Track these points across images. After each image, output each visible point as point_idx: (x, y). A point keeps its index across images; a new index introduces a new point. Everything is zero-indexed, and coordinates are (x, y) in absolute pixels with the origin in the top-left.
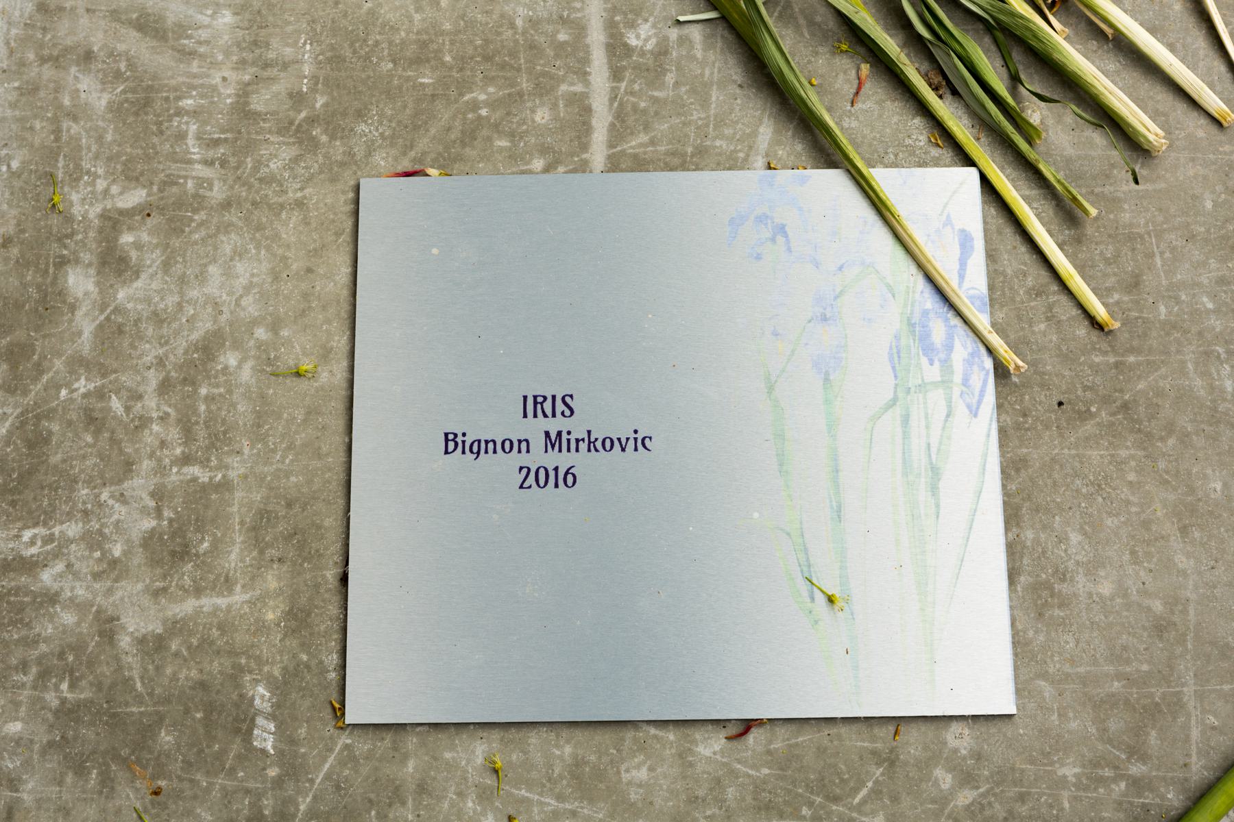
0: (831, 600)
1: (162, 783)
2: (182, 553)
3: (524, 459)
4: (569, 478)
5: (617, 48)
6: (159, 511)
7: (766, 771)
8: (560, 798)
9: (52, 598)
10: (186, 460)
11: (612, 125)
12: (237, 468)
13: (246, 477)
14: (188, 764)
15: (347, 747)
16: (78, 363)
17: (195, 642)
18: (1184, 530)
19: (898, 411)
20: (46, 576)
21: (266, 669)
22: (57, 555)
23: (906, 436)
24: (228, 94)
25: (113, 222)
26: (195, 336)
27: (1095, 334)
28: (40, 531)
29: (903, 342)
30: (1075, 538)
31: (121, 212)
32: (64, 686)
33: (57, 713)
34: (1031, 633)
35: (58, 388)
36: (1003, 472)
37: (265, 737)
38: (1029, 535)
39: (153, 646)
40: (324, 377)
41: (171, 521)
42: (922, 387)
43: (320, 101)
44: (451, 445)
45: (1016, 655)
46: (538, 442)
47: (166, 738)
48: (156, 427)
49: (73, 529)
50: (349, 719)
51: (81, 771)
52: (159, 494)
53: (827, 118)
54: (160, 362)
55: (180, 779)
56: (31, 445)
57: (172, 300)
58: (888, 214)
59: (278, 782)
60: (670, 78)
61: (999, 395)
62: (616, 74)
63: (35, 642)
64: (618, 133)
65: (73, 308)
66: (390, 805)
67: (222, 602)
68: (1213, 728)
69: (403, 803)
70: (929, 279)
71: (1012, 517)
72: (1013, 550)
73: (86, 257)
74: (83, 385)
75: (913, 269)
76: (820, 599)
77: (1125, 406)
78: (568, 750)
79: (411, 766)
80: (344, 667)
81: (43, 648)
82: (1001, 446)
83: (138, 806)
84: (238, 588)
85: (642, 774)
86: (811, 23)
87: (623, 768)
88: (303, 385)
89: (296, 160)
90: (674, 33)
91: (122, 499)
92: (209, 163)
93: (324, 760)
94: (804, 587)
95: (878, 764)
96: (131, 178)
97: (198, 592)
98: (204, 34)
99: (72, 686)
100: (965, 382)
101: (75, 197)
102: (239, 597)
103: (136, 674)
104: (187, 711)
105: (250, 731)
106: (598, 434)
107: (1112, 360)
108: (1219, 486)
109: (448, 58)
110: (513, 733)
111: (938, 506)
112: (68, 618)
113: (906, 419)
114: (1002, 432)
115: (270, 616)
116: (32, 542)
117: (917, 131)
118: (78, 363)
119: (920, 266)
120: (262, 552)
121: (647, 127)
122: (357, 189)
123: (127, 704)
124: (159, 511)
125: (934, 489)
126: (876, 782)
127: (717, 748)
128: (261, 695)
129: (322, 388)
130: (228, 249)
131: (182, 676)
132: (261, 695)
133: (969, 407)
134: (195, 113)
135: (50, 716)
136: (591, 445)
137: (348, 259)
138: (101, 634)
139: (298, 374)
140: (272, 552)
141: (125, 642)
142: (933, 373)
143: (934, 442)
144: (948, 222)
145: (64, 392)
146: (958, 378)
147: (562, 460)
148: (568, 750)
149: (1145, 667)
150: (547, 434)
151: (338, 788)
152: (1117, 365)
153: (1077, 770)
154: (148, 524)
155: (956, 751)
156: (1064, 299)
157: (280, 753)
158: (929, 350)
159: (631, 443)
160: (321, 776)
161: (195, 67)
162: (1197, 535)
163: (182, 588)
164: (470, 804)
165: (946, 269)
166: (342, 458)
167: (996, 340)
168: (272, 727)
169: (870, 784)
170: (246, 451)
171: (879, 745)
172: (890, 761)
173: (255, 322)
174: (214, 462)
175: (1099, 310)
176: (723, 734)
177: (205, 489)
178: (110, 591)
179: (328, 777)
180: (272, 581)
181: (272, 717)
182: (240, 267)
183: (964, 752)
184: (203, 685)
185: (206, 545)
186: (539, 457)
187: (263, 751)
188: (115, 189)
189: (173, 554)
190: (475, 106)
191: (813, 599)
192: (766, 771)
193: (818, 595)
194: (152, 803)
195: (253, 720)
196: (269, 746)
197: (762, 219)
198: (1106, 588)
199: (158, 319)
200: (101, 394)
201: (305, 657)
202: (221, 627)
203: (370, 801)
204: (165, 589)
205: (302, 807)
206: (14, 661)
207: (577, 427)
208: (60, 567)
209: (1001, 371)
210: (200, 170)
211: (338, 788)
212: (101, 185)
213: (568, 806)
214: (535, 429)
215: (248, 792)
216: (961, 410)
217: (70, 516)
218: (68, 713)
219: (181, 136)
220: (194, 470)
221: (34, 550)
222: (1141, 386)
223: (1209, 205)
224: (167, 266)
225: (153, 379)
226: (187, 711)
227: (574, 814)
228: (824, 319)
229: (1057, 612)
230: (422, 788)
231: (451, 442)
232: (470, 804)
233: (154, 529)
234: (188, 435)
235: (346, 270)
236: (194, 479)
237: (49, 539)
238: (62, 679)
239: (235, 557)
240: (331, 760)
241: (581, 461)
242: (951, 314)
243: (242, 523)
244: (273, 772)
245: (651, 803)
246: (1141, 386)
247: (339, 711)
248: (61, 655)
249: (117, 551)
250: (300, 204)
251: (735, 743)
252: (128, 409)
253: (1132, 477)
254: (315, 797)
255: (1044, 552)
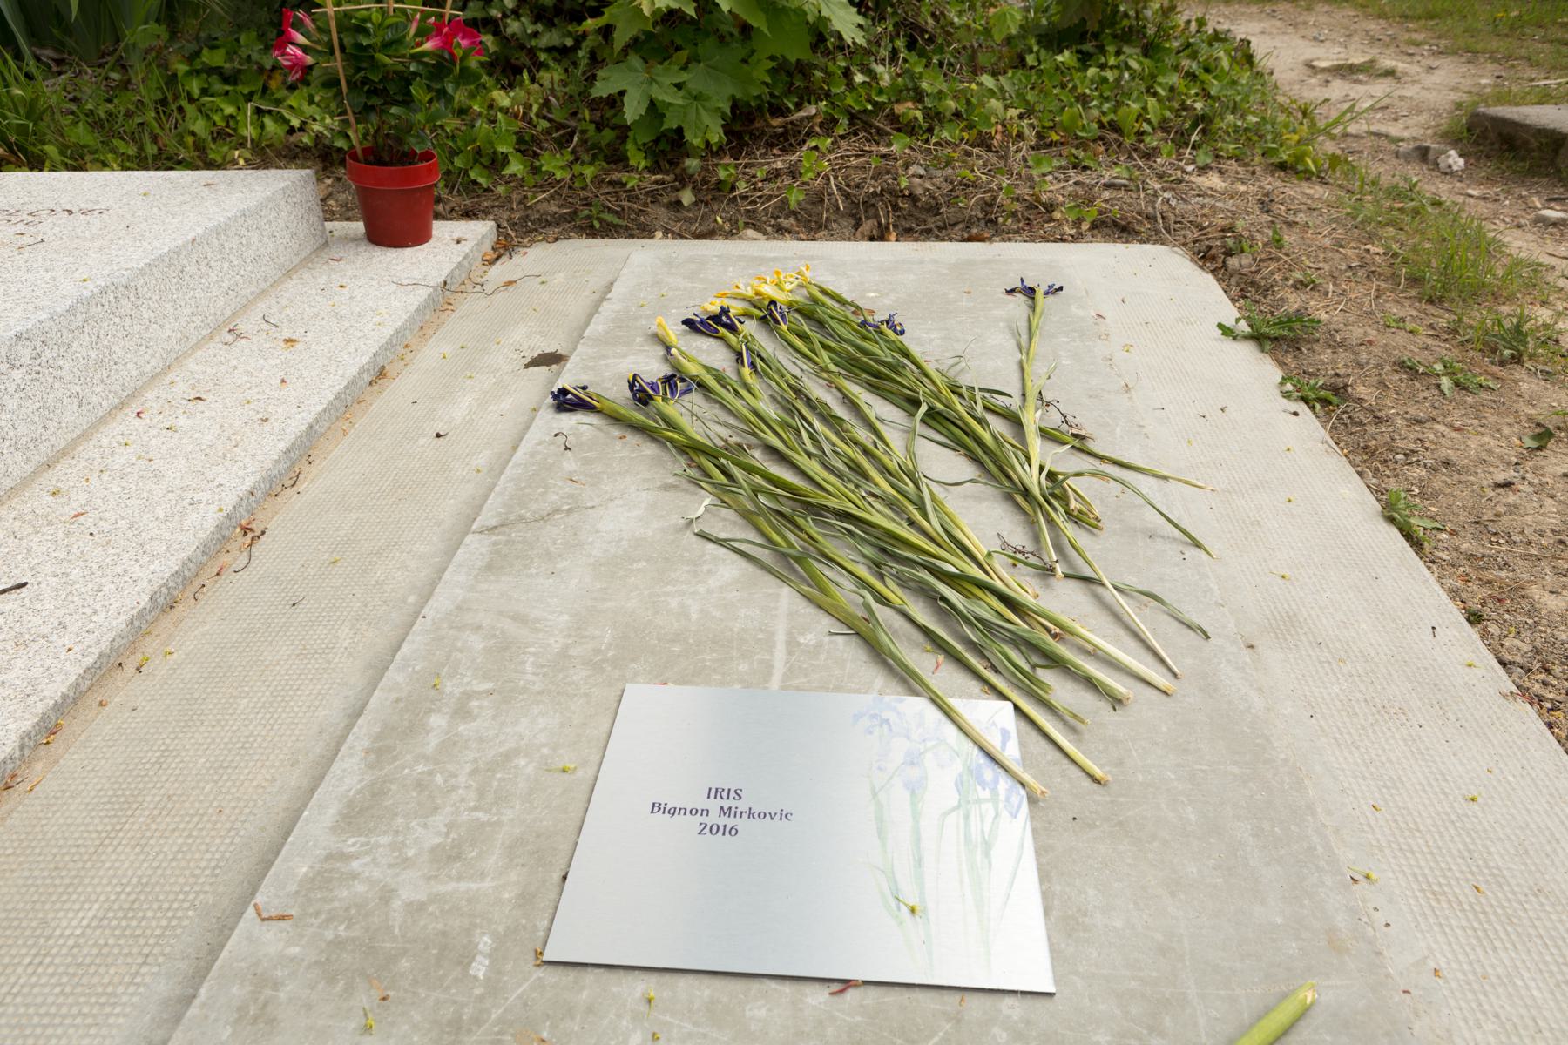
0: (913, 911)
1: (391, 993)
2: (457, 857)
3: (704, 819)
4: (733, 831)
5: (792, 644)
6: (447, 834)
7: (858, 1018)
8: (695, 1024)
9: (354, 876)
10: (476, 809)
11: (785, 674)
12: (508, 815)
13: (512, 820)
14: (415, 982)
15: (539, 978)
16: (426, 758)
17: (447, 907)
18: (1173, 894)
19: (961, 812)
20: (355, 865)
21: (493, 926)
22: (367, 853)
23: (967, 825)
24: (556, 648)
25: (468, 696)
26: (501, 750)
27: (1095, 786)
28: (363, 839)
29: (965, 778)
30: (1091, 892)
31: (475, 692)
32: (342, 928)
33: (329, 944)
34: (1063, 946)
35: (404, 768)
36: (1036, 852)
37: (480, 969)
38: (1058, 888)
39: (415, 909)
40: (580, 773)
41: (454, 839)
42: (979, 801)
43: (610, 654)
44: (656, 809)
45: (1053, 958)
46: (715, 811)
47: (405, 964)
48: (460, 791)
49: (384, 840)
50: (546, 957)
51: (331, 980)
52: (450, 826)
53: (917, 669)
54: (476, 760)
55: (406, 991)
56: (374, 795)
57: (492, 733)
58: (954, 715)
59: (481, 998)
60: (822, 657)
61: (1031, 811)
62: (790, 653)
63: (332, 900)
64: (786, 677)
65: (428, 732)
66: (562, 1019)
67: (474, 886)
68: (1217, 1019)
69: (573, 1018)
70: (982, 749)
71: (1044, 876)
72: (1046, 896)
73: (445, 710)
74: (420, 768)
75: (971, 744)
76: (905, 910)
77: (1120, 823)
78: (707, 992)
79: (585, 995)
80: (550, 929)
81: (336, 904)
82: (1034, 839)
83: (367, 1007)
84: (489, 879)
85: (762, 1013)
86: (909, 639)
87: (747, 1008)
88: (566, 776)
89: (589, 676)
90: (827, 639)
91: (425, 826)
92: (534, 674)
93: (520, 986)
94: (893, 902)
95: (948, 1021)
96: (486, 677)
97: (460, 878)
98: (549, 623)
99: (348, 928)
100: (1008, 799)
101: (449, 684)
102: (487, 884)
103: (397, 924)
104: (427, 948)
105: (469, 964)
106: (756, 809)
107: (1108, 799)
108: (1195, 870)
109: (691, 641)
110: (667, 978)
111: (990, 863)
112: (361, 888)
113: (967, 817)
114: (1035, 831)
115: (506, 896)
116: (354, 845)
117: (975, 686)
118: (426, 758)
119: (976, 743)
120: (511, 860)
121: (806, 676)
122: (623, 691)
123: (384, 941)
124: (447, 834)
125: (987, 854)
126: (946, 1033)
127: (822, 999)
128: (485, 942)
129: (448, 75)
130: (536, 712)
131: (430, 927)
132: (485, 942)
133: (1010, 813)
134: (534, 654)
135: (323, 945)
136: (751, 815)
137: (610, 721)
138: (380, 899)
139: (564, 771)
140: (520, 861)
141: (396, 904)
142: (985, 794)
143: (987, 830)
144: (994, 724)
145: (406, 771)
146: (1002, 796)
147: (730, 822)
148: (707, 992)
149: (1154, 974)
150: (722, 808)
151: (525, 1005)
152: (1112, 802)
153: (1108, 1038)
154: (437, 840)
155: (1009, 1017)
156: (1073, 768)
157: (488, 979)
158: (983, 784)
159: (778, 816)
160: (515, 996)
161: (540, 635)
162: (1182, 897)
163: (449, 877)
164: (625, 1023)
165: (994, 741)
166: (581, 814)
167: (1027, 777)
168: (487, 962)
169: (941, 1034)
170: (518, 807)
171: (948, 1008)
172: (958, 1020)
173: (543, 745)
174: (494, 810)
175: (1098, 772)
176: (827, 991)
177: (483, 824)
178: (397, 875)
179: (520, 997)
180: (513, 876)
181: (489, 956)
182: (540, 720)
183: (1015, 1018)
184: (444, 934)
185: (474, 854)
186: (712, 818)
187: (476, 978)
188: (474, 682)
189: (449, 857)
190: (704, 660)
191: (899, 909)
192: (858, 1018)
193: (903, 907)
194: (379, 1006)
195: (474, 958)
196: (481, 975)
197: (874, 716)
198: (1118, 924)
199: (481, 740)
200: (431, 773)
201: (524, 922)
202: (469, 901)
203: (548, 1015)
204: (436, 876)
205: (494, 1016)
206: (311, 910)
207: (742, 805)
208: (368, 859)
209: (1032, 800)
210: (530, 677)
211: (525, 1005)
212: (466, 680)
213: (701, 1030)
214: (714, 805)
215: (455, 1002)
216: (1005, 814)
217: (385, 833)
218: (338, 944)
219: (524, 663)
220: (480, 815)
221: (352, 849)
222: (1130, 813)
223: (1164, 729)
224: (494, 717)
225: (468, 768)
226: (427, 948)
227: (705, 1036)
228: (912, 763)
229: (1082, 934)
230: (590, 1010)
231: (656, 807)
232: (625, 1023)
233: (439, 844)
234: (481, 794)
235: (607, 726)
236: (478, 819)
237: (367, 844)
238: (342, 923)
239: (492, 861)
240: (525, 986)
241: (742, 823)
242: (996, 767)
243: (502, 844)
244: (478, 991)
245: (767, 1033)
246: (1130, 813)
247: (538, 954)
248: (347, 909)
249: (410, 853)
250: (586, 695)
251: (835, 998)
252: (445, 781)
253: (1129, 861)
254: (505, 1011)
255: (1069, 898)
